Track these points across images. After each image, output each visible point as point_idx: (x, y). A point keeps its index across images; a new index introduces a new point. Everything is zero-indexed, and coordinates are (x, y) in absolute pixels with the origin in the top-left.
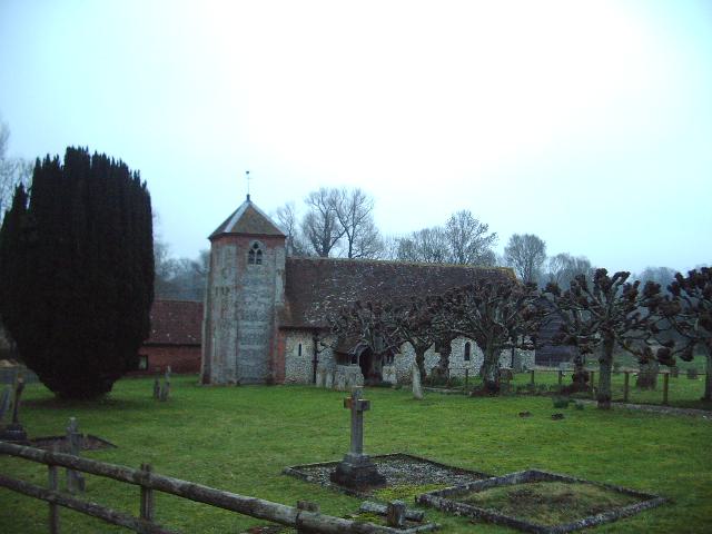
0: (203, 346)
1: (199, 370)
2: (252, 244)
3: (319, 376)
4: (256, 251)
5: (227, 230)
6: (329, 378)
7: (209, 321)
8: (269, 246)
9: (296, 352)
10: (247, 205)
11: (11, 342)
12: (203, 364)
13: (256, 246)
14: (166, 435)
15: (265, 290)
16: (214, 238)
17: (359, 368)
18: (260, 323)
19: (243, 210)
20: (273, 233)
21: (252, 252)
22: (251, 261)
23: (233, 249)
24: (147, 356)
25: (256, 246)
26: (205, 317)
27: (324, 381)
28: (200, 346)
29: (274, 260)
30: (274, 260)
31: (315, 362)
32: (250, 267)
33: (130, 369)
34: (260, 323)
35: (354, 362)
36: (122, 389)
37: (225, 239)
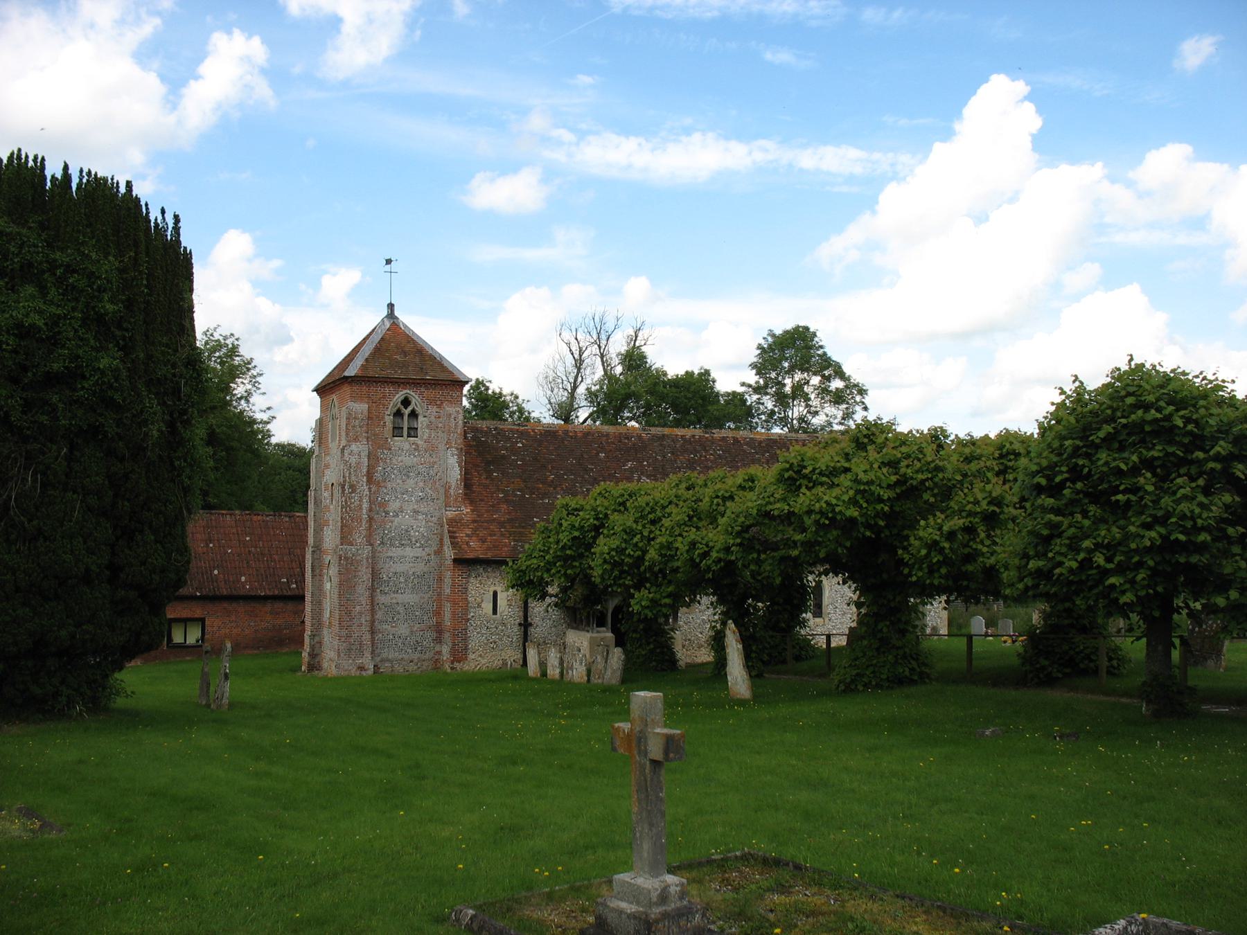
0: (308, 598)
1: (301, 643)
2: (399, 396)
3: (532, 655)
4: (407, 412)
5: (351, 371)
6: (553, 657)
7: (318, 548)
8: (431, 402)
9: (488, 607)
10: (388, 325)
11: (819, 588)
12: (308, 633)
13: (406, 402)
14: (167, 746)
15: (425, 479)
16: (323, 390)
17: (610, 635)
18: (419, 552)
19: (376, 338)
20: (442, 376)
21: (398, 414)
22: (397, 431)
23: (361, 407)
24: (202, 621)
25: (406, 402)
26: (311, 541)
27: (543, 665)
28: (301, 598)
29: (439, 426)
30: (439, 426)
31: (526, 625)
32: (420, 433)
33: (147, 642)
34: (419, 552)
35: (601, 623)
36: (138, 681)
37: (346, 390)
